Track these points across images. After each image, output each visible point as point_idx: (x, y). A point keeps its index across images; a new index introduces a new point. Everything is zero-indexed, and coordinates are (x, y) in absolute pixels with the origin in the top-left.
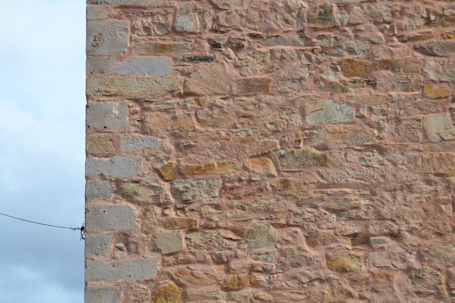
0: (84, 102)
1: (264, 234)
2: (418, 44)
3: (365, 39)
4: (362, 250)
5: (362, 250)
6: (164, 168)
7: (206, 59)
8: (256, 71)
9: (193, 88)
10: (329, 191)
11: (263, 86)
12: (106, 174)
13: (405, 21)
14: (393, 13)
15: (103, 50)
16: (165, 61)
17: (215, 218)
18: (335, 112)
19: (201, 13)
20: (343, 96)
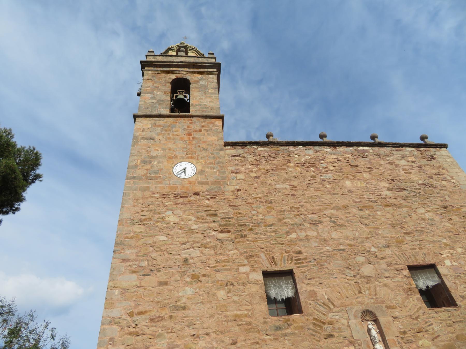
0: (99, 327)
1: (415, 228)
2: (214, 269)
3: (198, 268)
4: (326, 309)
5: (326, 309)
6: (130, 313)
7: (148, 275)
8: (163, 279)
9: (143, 284)
10: (185, 319)
11: (166, 283)
12: (109, 315)
13: (210, 262)
14: (206, 260)
15: (115, 273)
16: (135, 276)
17: (146, 331)
18: (189, 291)
19: (148, 261)
20: (191, 286)
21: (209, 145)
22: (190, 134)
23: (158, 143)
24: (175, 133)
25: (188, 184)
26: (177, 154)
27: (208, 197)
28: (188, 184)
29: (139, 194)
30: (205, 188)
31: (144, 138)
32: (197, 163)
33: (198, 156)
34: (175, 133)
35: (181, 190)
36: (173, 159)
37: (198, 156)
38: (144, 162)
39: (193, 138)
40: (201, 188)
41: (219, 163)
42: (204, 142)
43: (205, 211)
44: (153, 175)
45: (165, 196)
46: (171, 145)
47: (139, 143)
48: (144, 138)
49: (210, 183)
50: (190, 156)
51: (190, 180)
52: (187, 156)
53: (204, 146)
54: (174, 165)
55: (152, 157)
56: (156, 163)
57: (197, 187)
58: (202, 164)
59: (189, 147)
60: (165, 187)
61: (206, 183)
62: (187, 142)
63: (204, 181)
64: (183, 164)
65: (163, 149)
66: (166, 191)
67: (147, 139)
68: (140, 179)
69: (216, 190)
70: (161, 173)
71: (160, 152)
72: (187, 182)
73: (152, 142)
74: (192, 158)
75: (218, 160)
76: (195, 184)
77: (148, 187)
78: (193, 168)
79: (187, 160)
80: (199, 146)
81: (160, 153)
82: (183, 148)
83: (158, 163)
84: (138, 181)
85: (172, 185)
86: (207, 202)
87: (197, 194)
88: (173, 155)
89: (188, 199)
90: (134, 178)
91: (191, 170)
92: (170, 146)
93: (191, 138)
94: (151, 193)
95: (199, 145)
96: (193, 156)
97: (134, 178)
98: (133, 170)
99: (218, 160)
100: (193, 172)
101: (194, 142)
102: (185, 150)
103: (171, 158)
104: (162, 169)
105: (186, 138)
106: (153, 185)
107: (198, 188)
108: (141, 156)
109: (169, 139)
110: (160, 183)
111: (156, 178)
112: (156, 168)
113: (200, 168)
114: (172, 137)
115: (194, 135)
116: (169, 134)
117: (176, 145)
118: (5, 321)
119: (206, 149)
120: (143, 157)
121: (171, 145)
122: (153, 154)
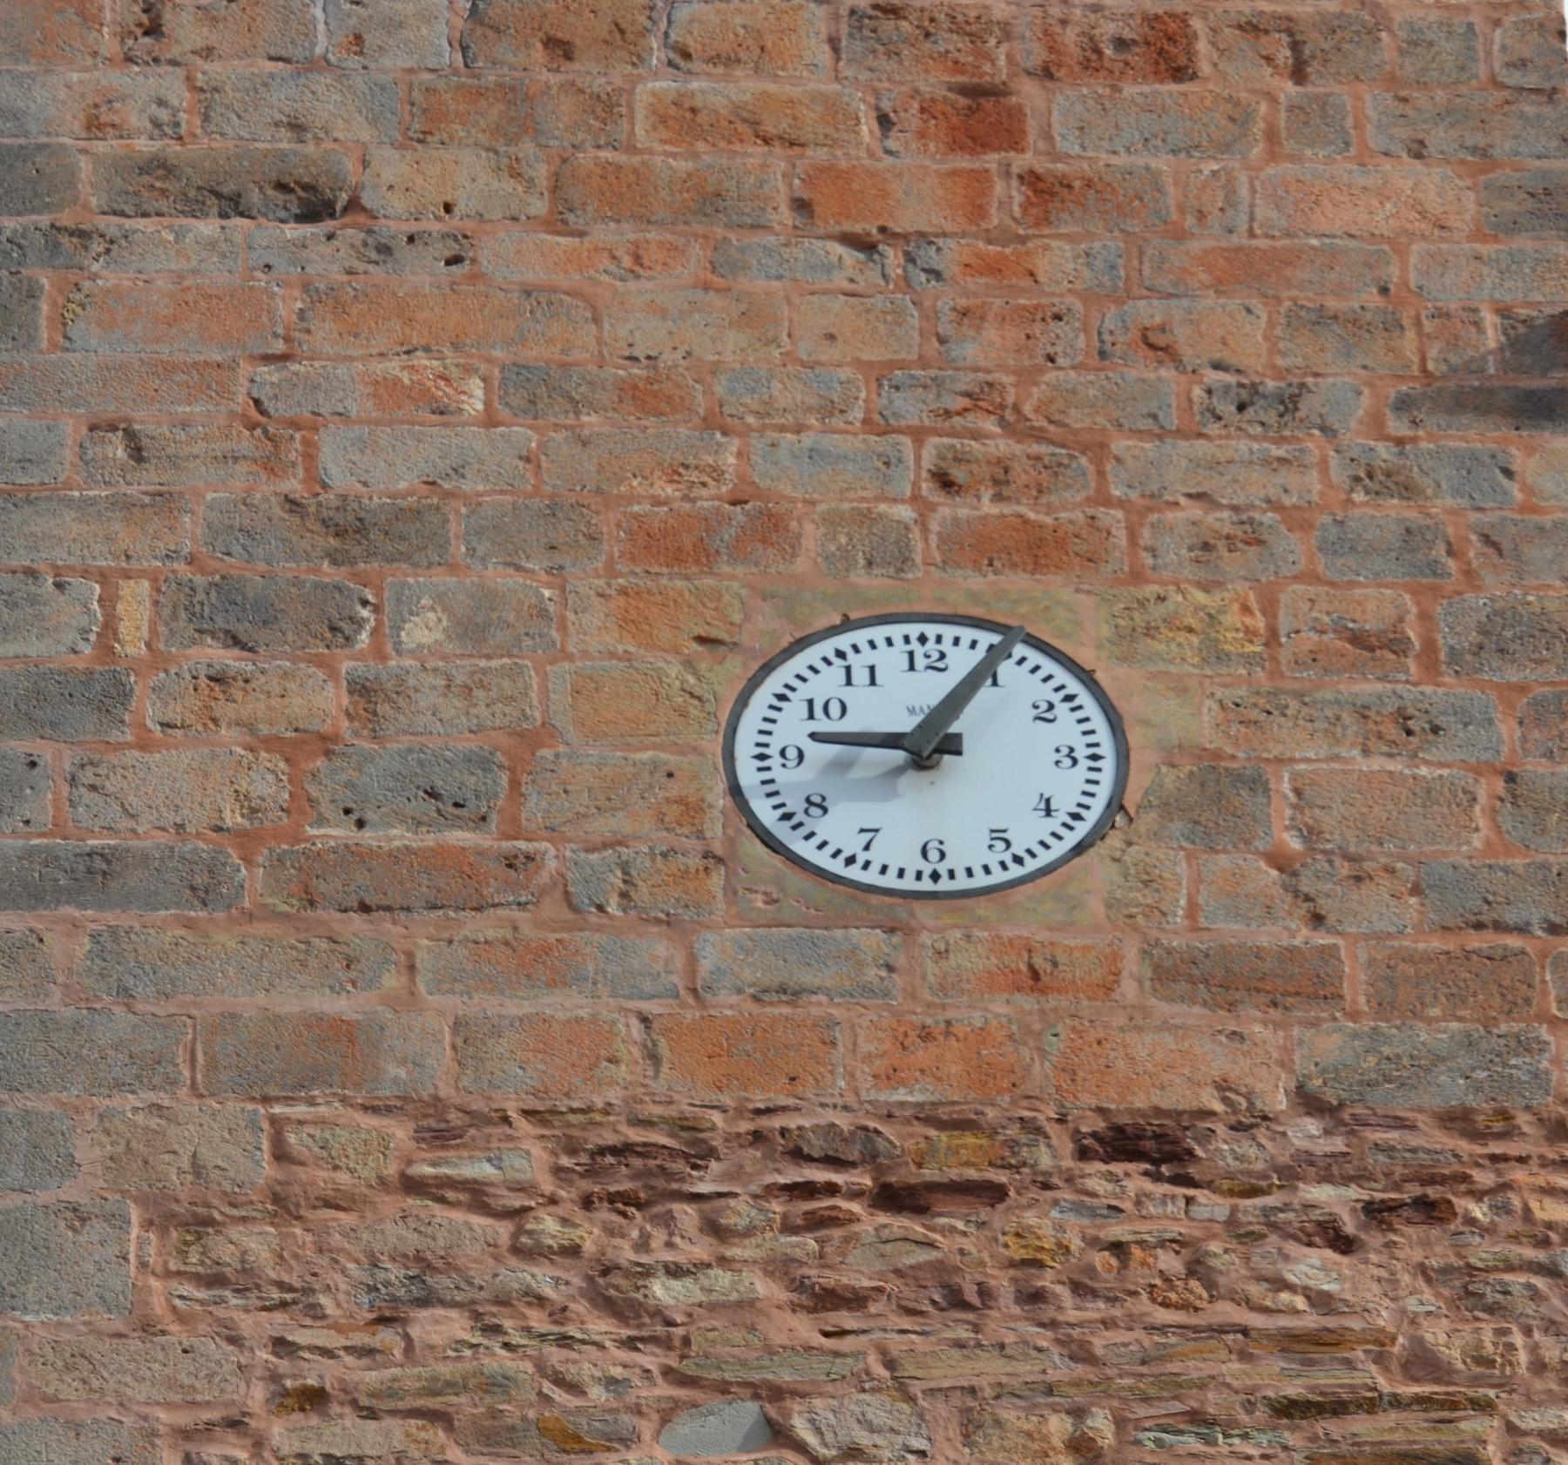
21: (1323, 318)
22: (980, 115)
23: (421, 273)
24: (711, 90)
25: (990, 982)
26: (783, 472)
27: (1333, 1199)
28: (990, 982)
29: (220, 1141)
30: (1266, 1058)
31: (163, 184)
32: (1129, 639)
33: (1136, 517)
34: (711, 90)
35: (891, 1077)
36: (721, 569)
37: (1136, 517)
38: (228, 612)
39: (1043, 191)
40: (1218, 1060)
41: (1500, 638)
42: (1243, 270)
43: (1288, 1409)
44: (400, 836)
45: (635, 1173)
46: (658, 315)
47: (106, 276)
48: (163, 184)
49: (1356, 987)
50: (1007, 532)
51: (1029, 923)
52: (948, 510)
53: (1248, 334)
54: (736, 669)
55: (350, 530)
56: (424, 631)
57: (1142, 1046)
58: (1216, 655)
59: (981, 350)
60: (607, 1023)
61: (1298, 986)
62: (949, 256)
63: (1268, 936)
64: (890, 661)
65: (533, 390)
66: (625, 1089)
67: (233, 205)
68: (203, 896)
69: (1451, 1089)
70: (534, 809)
71: (481, 448)
72: (972, 960)
73: (326, 253)
74: (1037, 550)
75: (1496, 586)
76: (1107, 989)
77: (339, 1032)
78: (1066, 730)
79: (970, 585)
80: (1156, 345)
81: (481, 448)
82: (880, 374)
83: (471, 629)
84: (159, 929)
85: (726, 1003)
86: (1312, 1266)
87: (1149, 1144)
88: (708, 499)
89: (998, 1218)
90: (97, 874)
91: (1026, 774)
92: (649, 335)
93: (1008, 196)
94: (400, 1132)
95: (1149, 311)
96: (1067, 508)
97: (97, 874)
98: (56, 756)
99: (1496, 586)
100: (1067, 788)
101: (1060, 260)
102: (910, 408)
103: (674, 546)
104: (548, 732)
105: (917, 182)
106: (428, 1009)
107: (1171, 1059)
108: (165, 501)
109: (626, 194)
110: (538, 964)
111: (458, 889)
112: (438, 723)
113: (1182, 715)
114: (670, 162)
115: (1064, 124)
116: (607, 107)
117: (753, 317)
118: (1561, 737)
119: (1289, 403)
120: (189, 531)
121: (658, 315)
122: (367, 466)
